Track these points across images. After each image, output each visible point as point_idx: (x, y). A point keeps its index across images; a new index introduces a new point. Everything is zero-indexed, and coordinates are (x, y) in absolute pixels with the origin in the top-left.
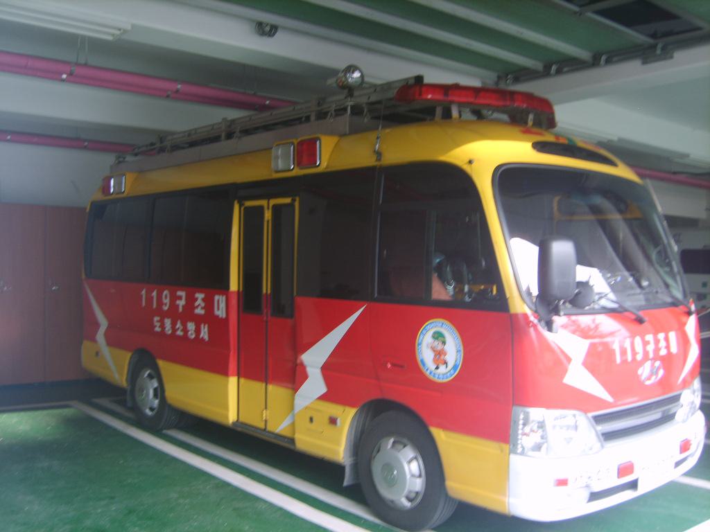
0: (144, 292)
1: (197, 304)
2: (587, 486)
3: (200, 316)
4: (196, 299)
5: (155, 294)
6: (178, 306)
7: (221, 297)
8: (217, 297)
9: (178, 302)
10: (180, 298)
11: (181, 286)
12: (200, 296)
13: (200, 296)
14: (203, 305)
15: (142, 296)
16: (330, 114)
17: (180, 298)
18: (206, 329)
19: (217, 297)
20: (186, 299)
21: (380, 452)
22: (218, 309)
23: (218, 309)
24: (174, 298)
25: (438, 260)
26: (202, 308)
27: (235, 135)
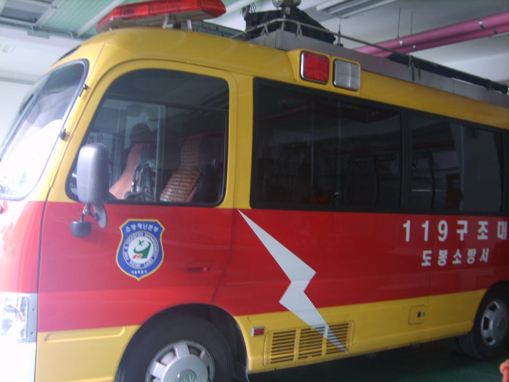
0: (407, 225)
1: (480, 231)
2: (424, 314)
3: (483, 241)
4: (480, 227)
5: (426, 225)
6: (459, 235)
7: (503, 223)
8: (499, 223)
9: (459, 231)
10: (461, 227)
11: (483, 215)
12: (483, 224)
13: (483, 224)
14: (486, 231)
15: (424, 229)
16: (263, 30)
17: (461, 227)
18: (487, 254)
19: (499, 223)
20: (469, 228)
21: (21, 331)
22: (501, 233)
23: (501, 233)
24: (453, 227)
25: (215, 161)
26: (485, 234)
27: (95, 29)
